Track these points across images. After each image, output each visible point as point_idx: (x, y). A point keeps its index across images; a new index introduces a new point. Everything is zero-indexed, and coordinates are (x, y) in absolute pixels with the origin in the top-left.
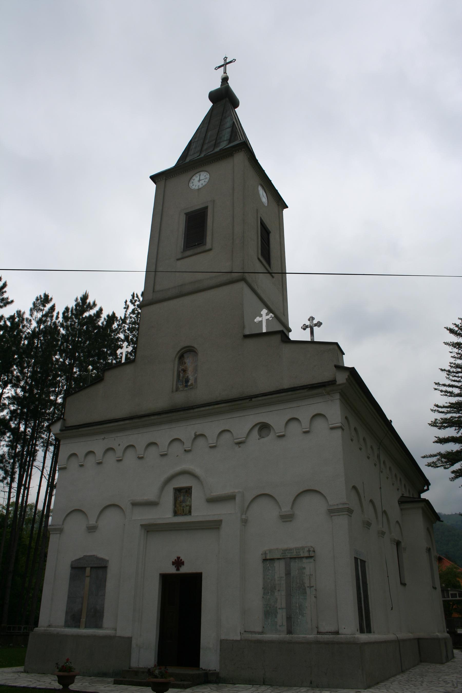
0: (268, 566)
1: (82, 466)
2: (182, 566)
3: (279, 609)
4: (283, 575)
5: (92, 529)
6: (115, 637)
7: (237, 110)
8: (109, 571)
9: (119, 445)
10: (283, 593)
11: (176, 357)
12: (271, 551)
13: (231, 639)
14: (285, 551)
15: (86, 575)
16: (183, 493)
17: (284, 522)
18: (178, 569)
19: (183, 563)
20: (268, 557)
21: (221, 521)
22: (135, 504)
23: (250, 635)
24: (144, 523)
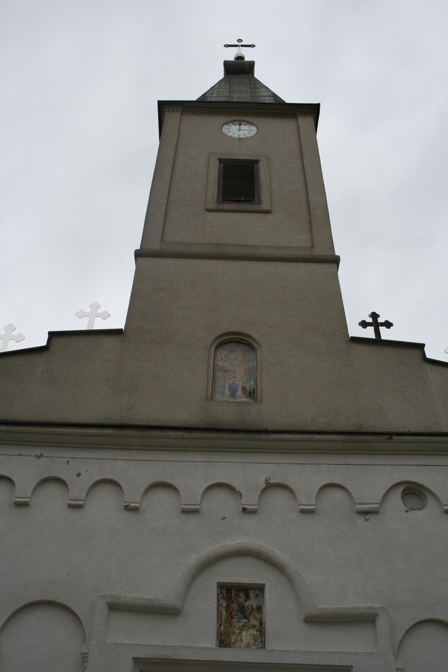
7: (139, 248)
9: (79, 475)
11: (212, 344)
22: (116, 607)
24: (143, 654)
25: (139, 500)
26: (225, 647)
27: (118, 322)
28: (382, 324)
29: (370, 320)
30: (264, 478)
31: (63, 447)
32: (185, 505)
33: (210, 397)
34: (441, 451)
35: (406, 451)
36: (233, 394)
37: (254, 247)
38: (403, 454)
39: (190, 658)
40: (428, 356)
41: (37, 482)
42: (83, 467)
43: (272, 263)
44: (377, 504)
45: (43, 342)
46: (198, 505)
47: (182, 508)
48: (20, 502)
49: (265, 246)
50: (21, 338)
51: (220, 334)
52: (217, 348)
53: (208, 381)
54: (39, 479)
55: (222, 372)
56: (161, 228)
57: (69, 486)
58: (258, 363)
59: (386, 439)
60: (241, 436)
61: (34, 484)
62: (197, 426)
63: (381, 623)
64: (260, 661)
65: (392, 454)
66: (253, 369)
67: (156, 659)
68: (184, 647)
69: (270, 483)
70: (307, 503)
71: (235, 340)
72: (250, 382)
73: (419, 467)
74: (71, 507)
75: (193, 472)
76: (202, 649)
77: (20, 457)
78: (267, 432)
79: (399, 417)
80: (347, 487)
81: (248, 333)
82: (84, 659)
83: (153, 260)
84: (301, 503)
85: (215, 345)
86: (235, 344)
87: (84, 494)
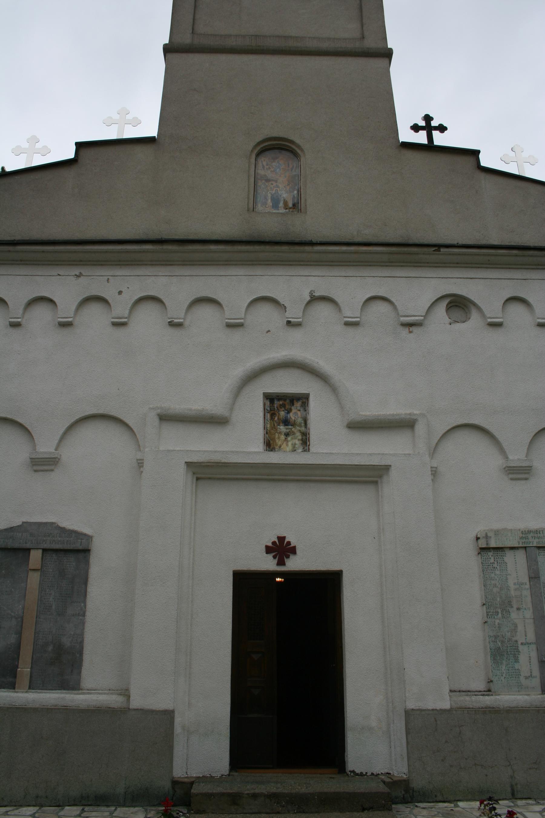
0: (492, 560)
1: (15, 325)
2: (292, 556)
3: (522, 644)
4: (526, 580)
5: (43, 464)
6: (125, 711)
7: (167, 42)
8: (94, 559)
9: (120, 293)
10: (529, 614)
11: (252, 151)
12: (497, 533)
13: (430, 708)
14: (526, 533)
15: (31, 566)
16: (284, 410)
17: (512, 479)
18: (281, 563)
19: (293, 551)
20: (493, 544)
21: (387, 468)
22: (165, 418)
23: (467, 698)
24: (195, 459)
25: (182, 315)
26: (272, 451)
27: (150, 128)
28: (436, 128)
29: (422, 123)
30: (309, 291)
31: (102, 265)
32: (229, 319)
33: (252, 209)
34: (489, 264)
35: (454, 263)
36: (275, 205)
37: (296, 38)
38: (450, 267)
39: (239, 462)
40: (483, 163)
41: (79, 301)
42: (123, 285)
43: (317, 58)
44: (422, 316)
45: (70, 154)
46: (243, 319)
47: (226, 322)
48: (64, 322)
49: (309, 38)
50: (46, 151)
51: (261, 139)
52: (258, 155)
53: (249, 191)
54: (80, 298)
55: (263, 181)
56: (192, 17)
57: (111, 304)
58: (302, 172)
59: (434, 251)
60: (285, 248)
61: (76, 304)
62: (239, 239)
63: (420, 428)
64: (304, 463)
65: (439, 267)
66: (297, 178)
67: (207, 463)
68: (232, 452)
69: (314, 296)
70: (352, 316)
71: (278, 146)
72: (293, 192)
73: (465, 280)
74: (115, 324)
75: (235, 286)
76: (250, 453)
77: (59, 277)
78: (311, 244)
79: (449, 228)
80: (393, 300)
81: (291, 139)
82: (140, 465)
83: (184, 55)
84: (345, 315)
85: (256, 151)
86: (276, 150)
87: (127, 312)
